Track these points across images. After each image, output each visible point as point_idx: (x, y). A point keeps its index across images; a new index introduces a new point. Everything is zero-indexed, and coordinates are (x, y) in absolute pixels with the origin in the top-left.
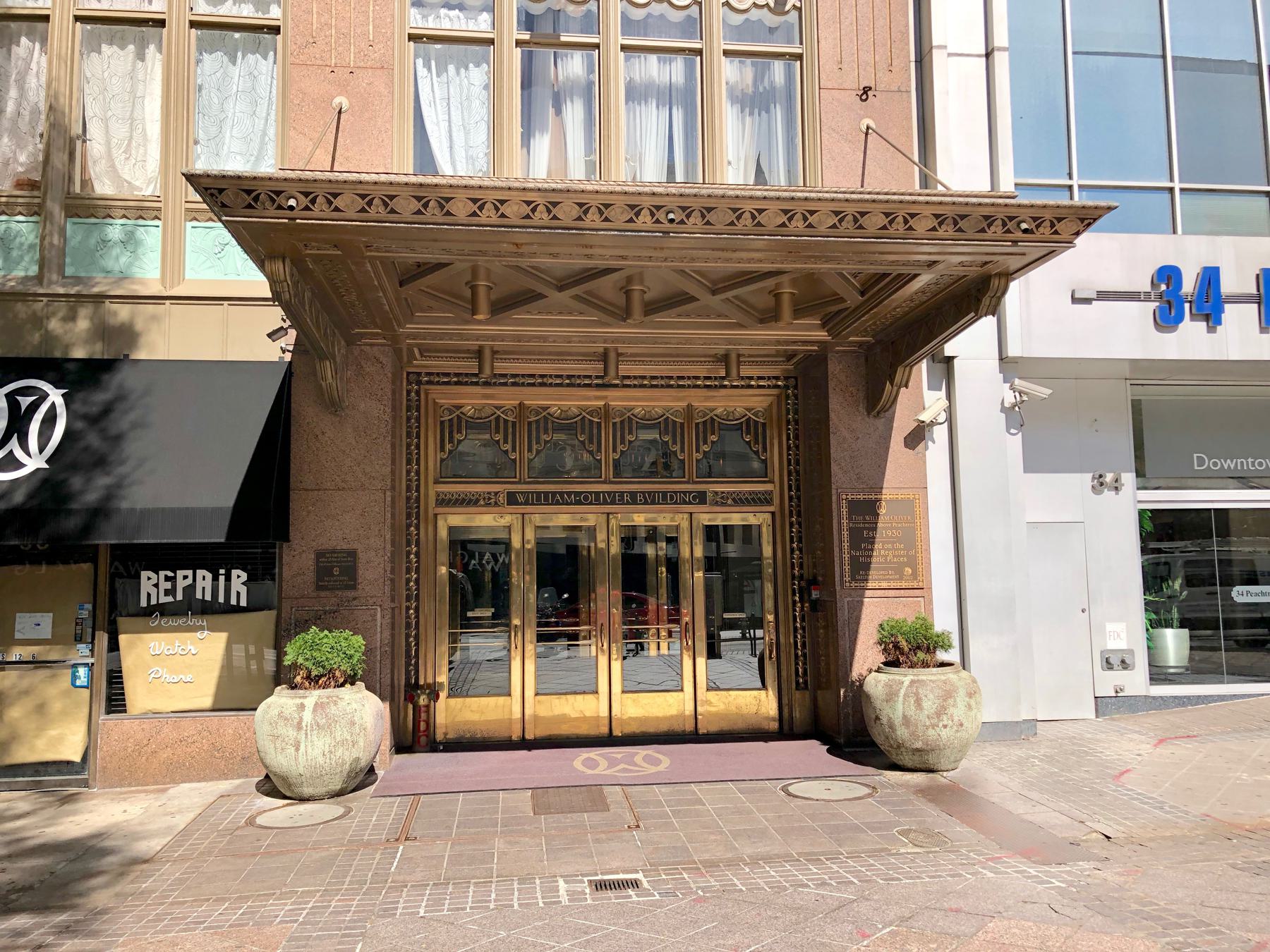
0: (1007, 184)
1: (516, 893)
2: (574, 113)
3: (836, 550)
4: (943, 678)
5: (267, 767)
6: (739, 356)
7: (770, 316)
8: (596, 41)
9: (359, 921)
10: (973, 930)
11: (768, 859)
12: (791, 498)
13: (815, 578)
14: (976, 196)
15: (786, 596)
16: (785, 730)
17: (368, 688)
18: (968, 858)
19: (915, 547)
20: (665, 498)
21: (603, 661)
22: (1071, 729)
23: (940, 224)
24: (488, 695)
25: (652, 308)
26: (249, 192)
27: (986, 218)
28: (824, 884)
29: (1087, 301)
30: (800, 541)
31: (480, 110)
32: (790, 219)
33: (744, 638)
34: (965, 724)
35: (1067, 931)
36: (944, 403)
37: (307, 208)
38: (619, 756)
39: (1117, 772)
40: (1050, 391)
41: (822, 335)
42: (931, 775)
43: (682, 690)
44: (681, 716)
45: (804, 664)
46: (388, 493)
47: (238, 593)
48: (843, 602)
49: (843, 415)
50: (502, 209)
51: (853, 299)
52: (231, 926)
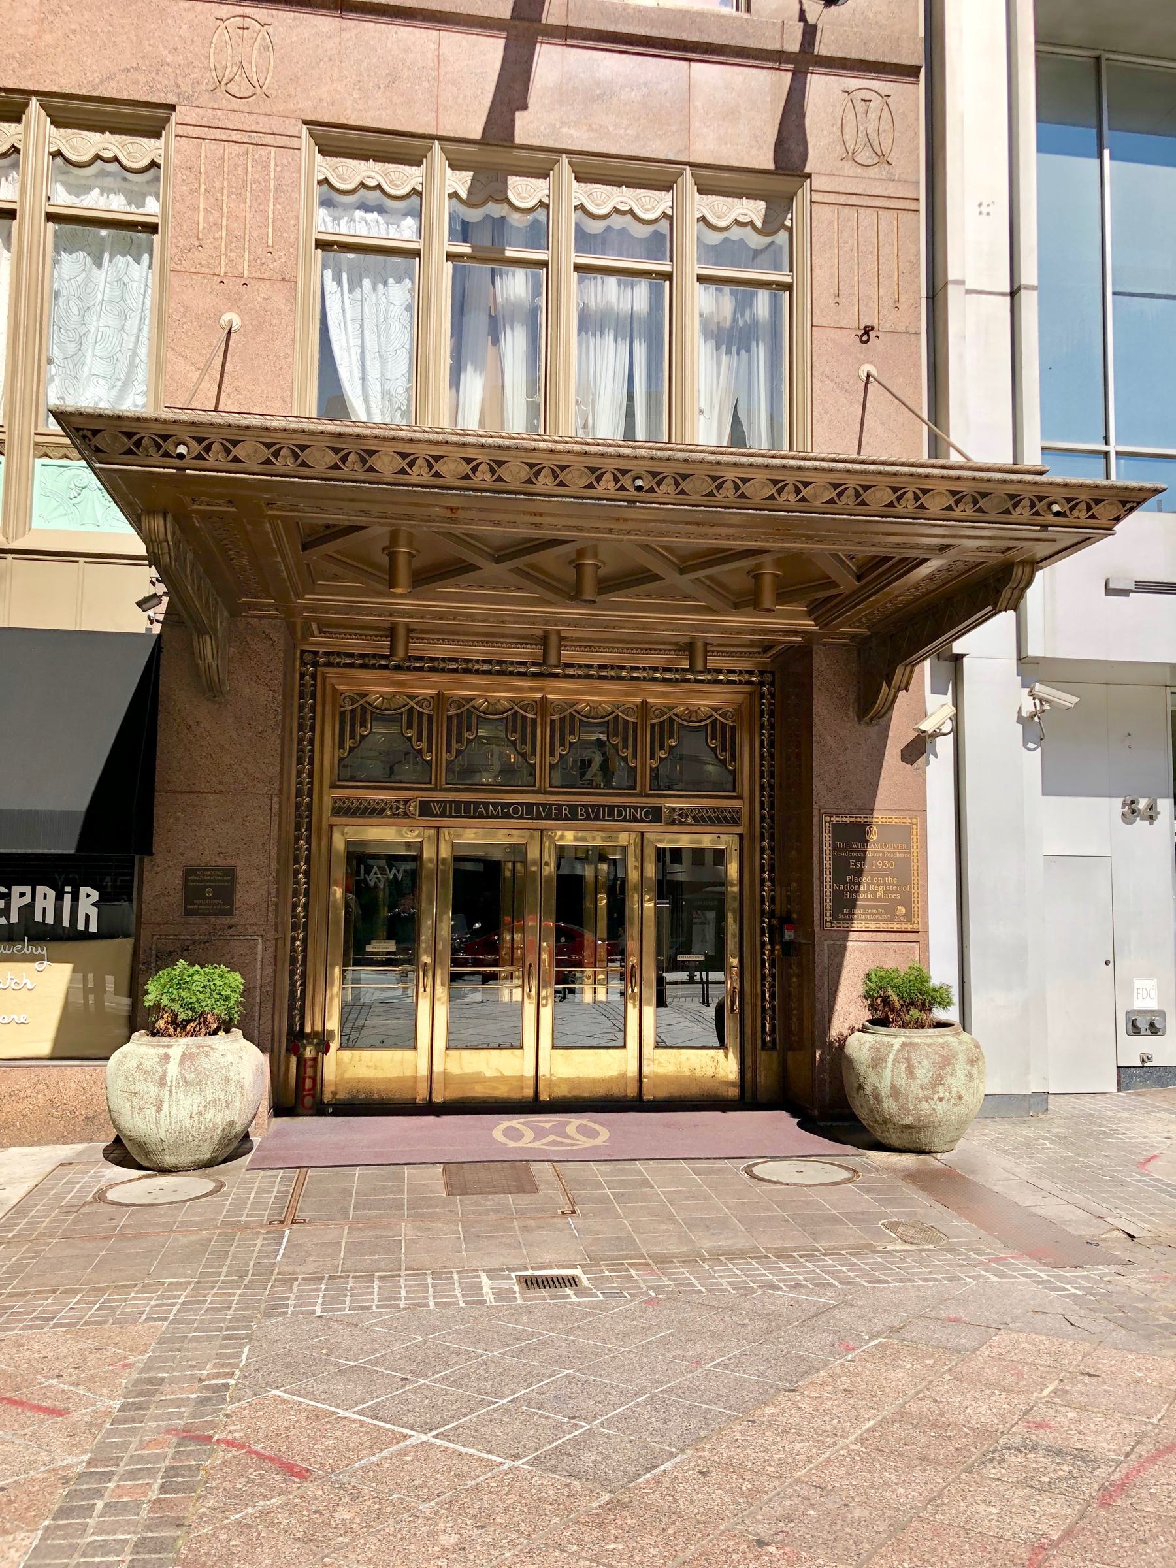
0: (1032, 457)
1: (431, 1290)
2: (514, 343)
3: (816, 883)
4: (940, 1040)
5: (118, 1129)
6: (706, 645)
7: (749, 600)
8: (544, 257)
9: (244, 1319)
10: (976, 1344)
11: (731, 1255)
12: (762, 818)
13: (789, 912)
14: (999, 471)
15: (753, 938)
16: (747, 1098)
17: (246, 1037)
18: (968, 1258)
19: (910, 882)
20: (611, 813)
21: (530, 1009)
22: (1088, 1106)
23: (957, 502)
24: (382, 1045)
25: (607, 585)
26: (129, 435)
27: (1012, 497)
28: (798, 1286)
29: (1124, 593)
30: (772, 870)
31: (400, 338)
32: (780, 491)
33: (691, 980)
34: (965, 1097)
35: (1083, 1347)
36: (950, 710)
37: (199, 457)
38: (547, 1126)
39: (1141, 1159)
40: (1076, 700)
41: (808, 624)
42: (922, 1157)
43: (624, 1047)
44: (624, 1076)
45: (773, 1018)
46: (276, 799)
47: (87, 916)
48: (822, 947)
49: (827, 714)
50: (437, 467)
51: (847, 583)
52: (86, 1323)
